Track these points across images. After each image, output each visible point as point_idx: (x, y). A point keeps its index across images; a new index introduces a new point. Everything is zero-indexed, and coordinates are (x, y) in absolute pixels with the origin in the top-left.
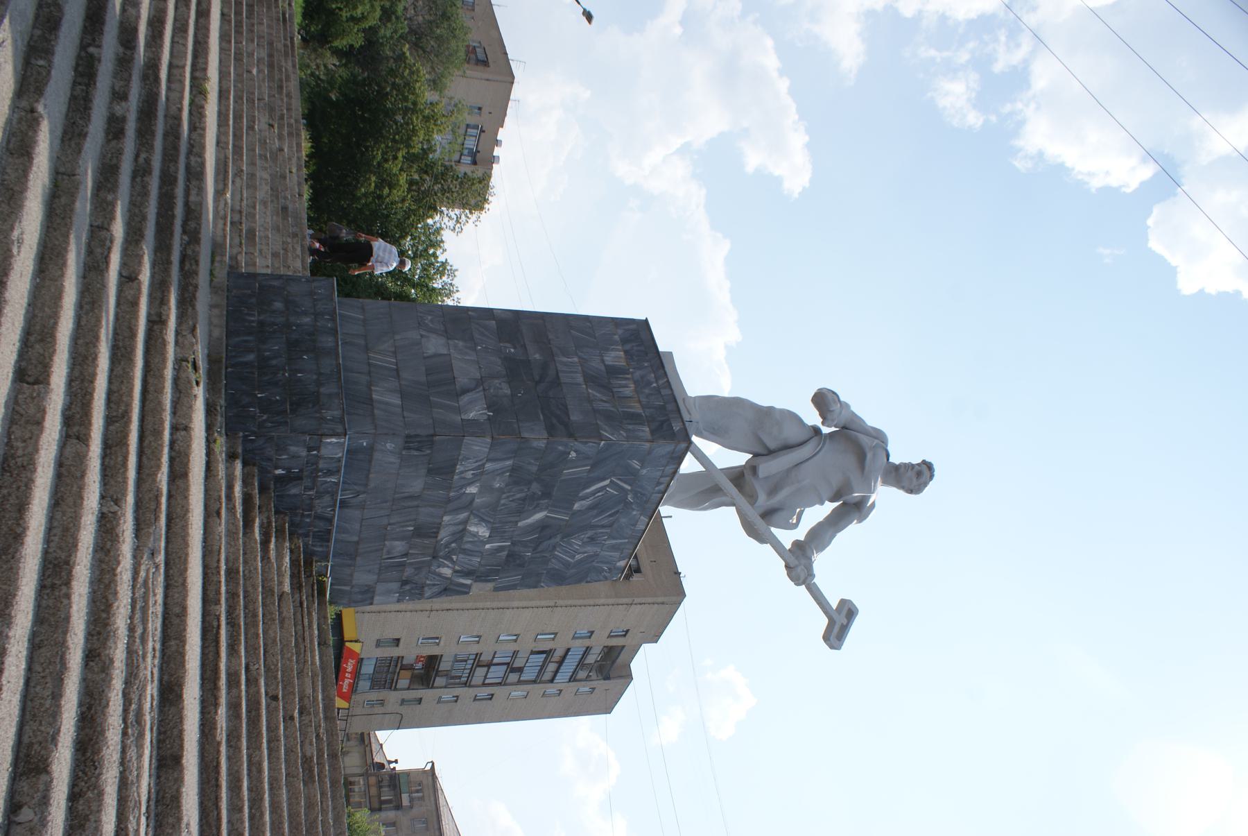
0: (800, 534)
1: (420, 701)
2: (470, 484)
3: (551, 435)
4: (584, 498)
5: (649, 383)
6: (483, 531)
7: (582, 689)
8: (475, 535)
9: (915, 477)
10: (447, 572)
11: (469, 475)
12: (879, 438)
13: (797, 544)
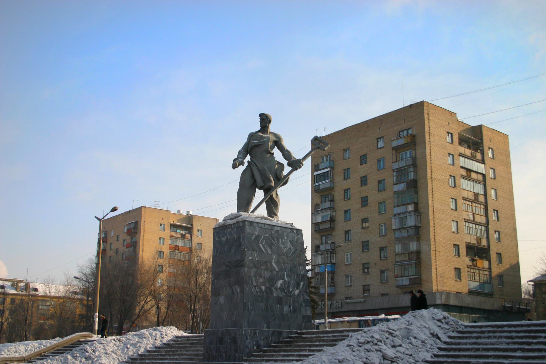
0: (285, 162)
1: (499, 255)
2: (261, 289)
3: (243, 266)
4: (266, 251)
5: (230, 231)
6: (280, 282)
7: (490, 155)
8: (281, 285)
9: (265, 120)
10: (297, 292)
11: (258, 290)
12: (252, 136)
13: (289, 165)
